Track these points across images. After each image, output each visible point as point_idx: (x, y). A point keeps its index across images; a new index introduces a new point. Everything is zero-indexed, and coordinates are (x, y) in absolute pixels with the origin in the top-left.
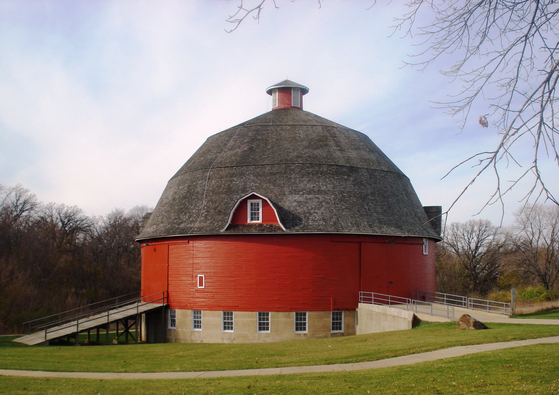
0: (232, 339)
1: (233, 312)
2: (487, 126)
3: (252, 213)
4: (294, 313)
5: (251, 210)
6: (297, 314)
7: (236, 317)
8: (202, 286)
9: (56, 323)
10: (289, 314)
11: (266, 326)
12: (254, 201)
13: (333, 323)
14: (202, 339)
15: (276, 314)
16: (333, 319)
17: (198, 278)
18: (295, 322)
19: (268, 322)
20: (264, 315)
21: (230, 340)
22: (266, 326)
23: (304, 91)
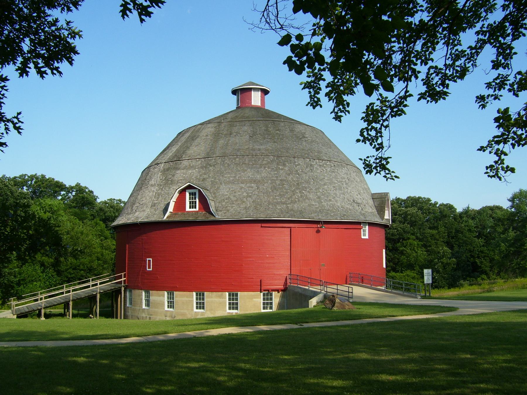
0: (173, 316)
1: (239, 292)
2: (445, 100)
3: (190, 202)
4: (227, 294)
5: (190, 199)
6: (229, 295)
7: (176, 297)
8: (150, 268)
9: (306, 325)
10: (222, 294)
11: (235, 306)
12: (192, 191)
13: (264, 304)
14: (150, 316)
15: (211, 295)
16: (264, 299)
17: (147, 261)
18: (262, 301)
19: (192, 299)
20: (233, 296)
21: (172, 317)
22: (235, 306)
23: (36, 174)
